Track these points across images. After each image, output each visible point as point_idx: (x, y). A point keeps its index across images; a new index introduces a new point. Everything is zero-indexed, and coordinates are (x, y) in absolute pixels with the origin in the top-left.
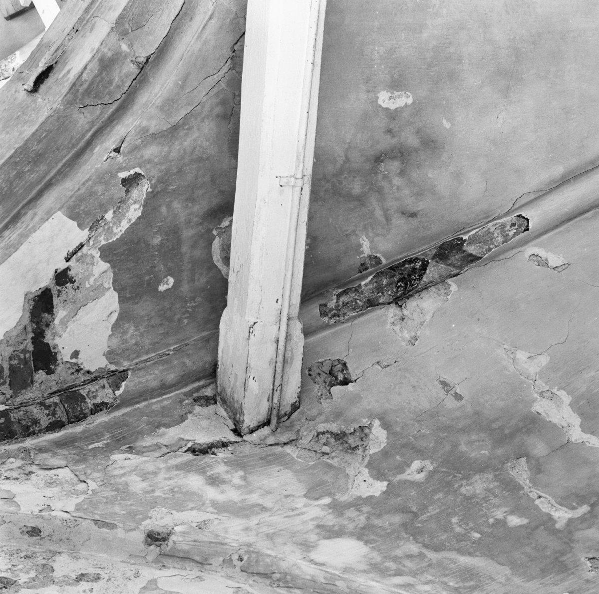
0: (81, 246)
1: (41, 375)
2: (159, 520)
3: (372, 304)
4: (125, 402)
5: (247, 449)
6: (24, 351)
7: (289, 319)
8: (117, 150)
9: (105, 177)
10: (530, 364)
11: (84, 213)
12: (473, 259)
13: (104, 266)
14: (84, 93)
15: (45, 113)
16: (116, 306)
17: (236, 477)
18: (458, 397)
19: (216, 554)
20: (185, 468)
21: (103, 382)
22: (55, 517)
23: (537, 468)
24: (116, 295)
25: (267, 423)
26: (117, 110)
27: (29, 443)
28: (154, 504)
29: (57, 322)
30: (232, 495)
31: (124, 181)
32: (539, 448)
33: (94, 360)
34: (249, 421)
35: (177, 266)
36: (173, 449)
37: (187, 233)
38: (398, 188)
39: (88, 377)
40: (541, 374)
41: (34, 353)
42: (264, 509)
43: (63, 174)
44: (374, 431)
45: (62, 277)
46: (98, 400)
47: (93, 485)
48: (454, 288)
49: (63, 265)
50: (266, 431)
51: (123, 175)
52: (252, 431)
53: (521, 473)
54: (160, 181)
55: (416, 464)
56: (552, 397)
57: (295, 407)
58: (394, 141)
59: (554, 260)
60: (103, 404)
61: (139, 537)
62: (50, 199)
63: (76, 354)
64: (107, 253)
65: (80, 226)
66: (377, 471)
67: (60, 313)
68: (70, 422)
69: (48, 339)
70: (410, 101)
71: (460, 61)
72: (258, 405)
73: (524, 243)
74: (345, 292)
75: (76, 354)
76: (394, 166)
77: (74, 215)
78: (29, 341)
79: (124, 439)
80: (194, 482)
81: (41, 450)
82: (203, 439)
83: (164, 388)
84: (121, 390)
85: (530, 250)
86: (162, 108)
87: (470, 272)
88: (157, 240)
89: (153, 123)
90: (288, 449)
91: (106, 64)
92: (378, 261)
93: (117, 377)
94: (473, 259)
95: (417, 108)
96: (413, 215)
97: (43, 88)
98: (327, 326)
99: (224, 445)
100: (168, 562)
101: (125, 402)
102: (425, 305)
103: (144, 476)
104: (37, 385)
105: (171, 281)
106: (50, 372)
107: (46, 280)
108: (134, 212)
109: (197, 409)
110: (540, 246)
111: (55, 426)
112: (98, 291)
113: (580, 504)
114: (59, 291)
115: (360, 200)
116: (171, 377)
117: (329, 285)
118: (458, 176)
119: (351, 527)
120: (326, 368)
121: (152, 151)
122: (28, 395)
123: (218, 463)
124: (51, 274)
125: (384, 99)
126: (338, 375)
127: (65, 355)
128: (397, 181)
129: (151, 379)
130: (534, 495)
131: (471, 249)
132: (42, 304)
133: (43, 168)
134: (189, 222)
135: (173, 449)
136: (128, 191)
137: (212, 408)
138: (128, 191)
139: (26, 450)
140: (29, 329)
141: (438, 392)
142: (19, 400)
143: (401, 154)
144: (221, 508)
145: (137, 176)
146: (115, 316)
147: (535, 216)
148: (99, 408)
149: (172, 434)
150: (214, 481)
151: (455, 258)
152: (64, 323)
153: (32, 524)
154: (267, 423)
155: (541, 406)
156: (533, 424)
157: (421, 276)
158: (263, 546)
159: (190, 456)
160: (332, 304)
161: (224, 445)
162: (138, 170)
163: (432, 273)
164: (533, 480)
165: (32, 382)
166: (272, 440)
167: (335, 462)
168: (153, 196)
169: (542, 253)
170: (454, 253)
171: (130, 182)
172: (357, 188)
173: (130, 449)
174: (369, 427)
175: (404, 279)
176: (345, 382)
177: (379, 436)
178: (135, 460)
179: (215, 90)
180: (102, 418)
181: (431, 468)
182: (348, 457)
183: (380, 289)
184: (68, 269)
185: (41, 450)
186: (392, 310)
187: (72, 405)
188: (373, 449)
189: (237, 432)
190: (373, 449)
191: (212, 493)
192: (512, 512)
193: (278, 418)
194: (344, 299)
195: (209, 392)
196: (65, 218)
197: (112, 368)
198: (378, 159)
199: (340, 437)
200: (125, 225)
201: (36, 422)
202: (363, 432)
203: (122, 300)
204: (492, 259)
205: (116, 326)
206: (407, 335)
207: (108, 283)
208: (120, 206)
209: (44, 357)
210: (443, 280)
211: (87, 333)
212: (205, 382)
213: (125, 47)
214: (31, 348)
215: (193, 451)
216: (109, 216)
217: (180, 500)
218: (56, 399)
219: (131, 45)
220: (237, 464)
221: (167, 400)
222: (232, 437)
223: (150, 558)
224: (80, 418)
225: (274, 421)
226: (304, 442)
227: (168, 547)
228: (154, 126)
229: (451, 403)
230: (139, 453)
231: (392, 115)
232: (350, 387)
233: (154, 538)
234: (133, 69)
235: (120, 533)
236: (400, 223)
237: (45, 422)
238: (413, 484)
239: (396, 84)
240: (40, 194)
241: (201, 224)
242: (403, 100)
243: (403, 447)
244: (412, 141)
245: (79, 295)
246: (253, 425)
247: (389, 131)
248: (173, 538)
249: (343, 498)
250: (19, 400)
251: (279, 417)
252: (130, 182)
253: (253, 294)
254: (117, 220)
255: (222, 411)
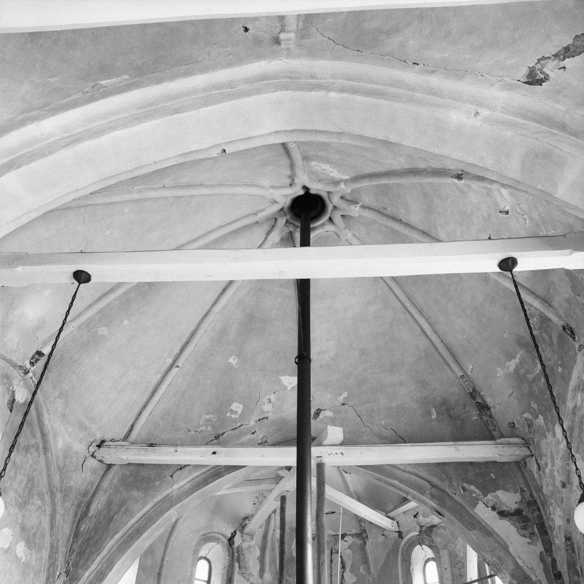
0: (484, 503)
1: (524, 513)
2: (559, 484)
3: (491, 416)
4: (529, 488)
5: (537, 454)
6: (517, 519)
7: (496, 444)
8: (455, 494)
9: (463, 497)
10: (500, 373)
11: (474, 503)
12: (474, 389)
13: (489, 495)
14: (442, 503)
15: (448, 514)
16: (501, 491)
17: (545, 458)
18: (513, 392)
19: (566, 468)
20: (544, 473)
21: (524, 494)
22: (563, 515)
23: (528, 372)
24: (497, 492)
25: (528, 447)
26: (446, 493)
27: (545, 517)
28: (554, 484)
29: (507, 509)
30: (549, 460)
31: (464, 491)
32: (522, 371)
33: (517, 497)
34: (528, 453)
35: (484, 475)
36: (540, 476)
37: (478, 471)
38: (458, 410)
39: (523, 498)
40: (502, 369)
41: (518, 515)
42: (551, 452)
43: (464, 508)
44: (526, 417)
45: (494, 508)
46: (529, 496)
47: (552, 501)
48: (483, 393)
49: (490, 508)
50: (531, 447)
51: (462, 492)
52: (531, 452)
53: (530, 376)
54: (463, 480)
55: (533, 405)
56: (508, 367)
57: (523, 439)
58: (445, 412)
59: (471, 367)
60: (530, 494)
61: (564, 490)
62: (472, 513)
63: (516, 503)
64: (485, 495)
65: (478, 504)
66: (537, 417)
67: (504, 508)
68: (537, 505)
69: (513, 512)
70: (434, 409)
71: (421, 397)
72: (523, 450)
73: (467, 375)
74: (488, 424)
75: (516, 503)
76: (452, 412)
77: (475, 506)
78: (514, 517)
79: (539, 489)
80: (547, 471)
81: (546, 514)
82: (536, 466)
83: (523, 476)
84: (526, 489)
85: (469, 373)
86: (443, 482)
87: (478, 389)
88: (480, 480)
89: (447, 484)
90: (535, 441)
91: (433, 497)
92: (479, 414)
93: (522, 491)
94: (474, 389)
95: (435, 407)
96: (464, 406)
97: (442, 513)
98: (499, 428)
99: (536, 460)
100: (571, 481)
101: (529, 488)
102: (489, 400)
103: (548, 485)
104: (527, 514)
105: (492, 474)
106: (523, 511)
107: (495, 513)
108: (473, 488)
109: (528, 466)
110: (467, 370)
111: (539, 509)
112: (497, 497)
113: (535, 361)
114: (498, 509)
115: (462, 420)
116: (519, 474)
117: (487, 432)
118: (452, 394)
119: (552, 427)
120: (511, 429)
121: (455, 484)
122: (530, 516)
123: (542, 463)
124: (493, 512)
125: (434, 417)
126: (512, 425)
127: (517, 506)
128: (456, 411)
129: (521, 481)
130: (535, 374)
131: (471, 390)
132: (502, 514)
133: (463, 514)
134: (474, 471)
135: (540, 476)
136: (467, 490)
137: (527, 462)
138: (467, 490)
139: (547, 518)
140: (510, 518)
141: (512, 398)
142: (532, 520)
143: (448, 410)
144: (553, 465)
145: (462, 487)
146: (504, 491)
147: (460, 374)
148: (532, 496)
149: (536, 475)
150: (546, 465)
151: (474, 394)
152: (507, 507)
153: (566, 521)
154: (528, 447)
155: (511, 369)
156: (516, 371)
157: (481, 403)
158: (561, 454)
159: (541, 471)
160: (492, 428)
161: (536, 460)
162: (460, 488)
163: (479, 400)
164: (532, 373)
165: (526, 516)
166: (533, 446)
167: (536, 428)
168: (468, 482)
169: (469, 370)
170: (474, 394)
171: (464, 489)
172: (459, 422)
173: (542, 488)
174: (525, 418)
175: (483, 407)
176: (514, 423)
177: (526, 415)
178: (544, 487)
179: (549, 146)
180: (535, 495)
181: (533, 402)
182: (534, 425)
183: (486, 415)
184: (491, 507)
185: (546, 514)
186: (492, 410)
187: (532, 503)
188: (531, 417)
189: (532, 456)
190: (531, 417)
191: (549, 467)
192: (541, 381)
193: (527, 444)
194: (490, 424)
195: (523, 462)
196: (476, 508)
197: (520, 491)
198: (450, 417)
199: (529, 426)
200: (476, 490)
201: (538, 515)
202: (526, 420)
203: (499, 489)
204: (472, 383)
205: (507, 491)
206: (498, 406)
207: (494, 494)
208: (471, 492)
209: (518, 512)
210: (481, 397)
211: (509, 499)
212: (520, 465)
213: (428, 492)
214: (516, 517)
215: (539, 469)
216: (474, 495)
217: (553, 476)
218: (531, 509)
219: (427, 490)
220: (541, 455)
221: (527, 475)
222: (534, 457)
223: (570, 486)
224: (536, 502)
225: (528, 445)
226: (532, 437)
227: (566, 482)
228: (448, 484)
229: (515, 394)
230: (542, 485)
231: (438, 414)
232: (515, 422)
233: (564, 485)
234: (433, 489)
235: (564, 496)
236: (467, 409)
237: (538, 513)
238: (538, 407)
239: (430, 414)
240: (471, 515)
241: (474, 467)
242: (434, 411)
243: (529, 409)
244: (444, 408)
245: (499, 503)
246: (529, 452)
247: (442, 414)
248: (562, 480)
249: (545, 428)
250: (532, 520)
251: (526, 444)
252: (464, 489)
253: (489, 455)
254: (475, 493)
255: (527, 460)
